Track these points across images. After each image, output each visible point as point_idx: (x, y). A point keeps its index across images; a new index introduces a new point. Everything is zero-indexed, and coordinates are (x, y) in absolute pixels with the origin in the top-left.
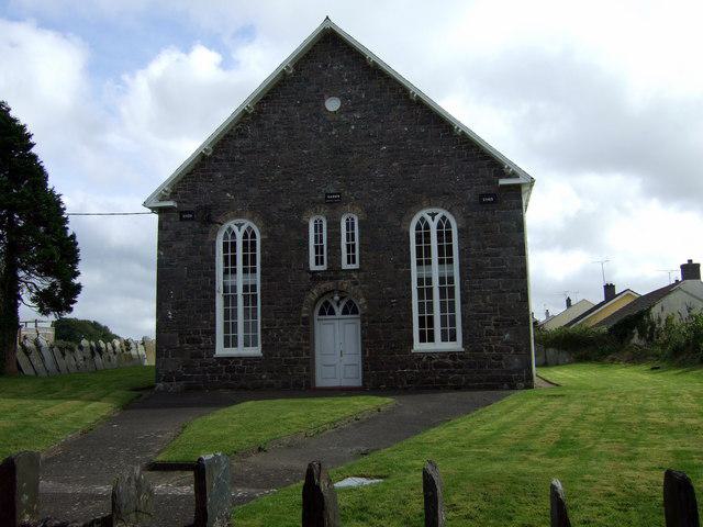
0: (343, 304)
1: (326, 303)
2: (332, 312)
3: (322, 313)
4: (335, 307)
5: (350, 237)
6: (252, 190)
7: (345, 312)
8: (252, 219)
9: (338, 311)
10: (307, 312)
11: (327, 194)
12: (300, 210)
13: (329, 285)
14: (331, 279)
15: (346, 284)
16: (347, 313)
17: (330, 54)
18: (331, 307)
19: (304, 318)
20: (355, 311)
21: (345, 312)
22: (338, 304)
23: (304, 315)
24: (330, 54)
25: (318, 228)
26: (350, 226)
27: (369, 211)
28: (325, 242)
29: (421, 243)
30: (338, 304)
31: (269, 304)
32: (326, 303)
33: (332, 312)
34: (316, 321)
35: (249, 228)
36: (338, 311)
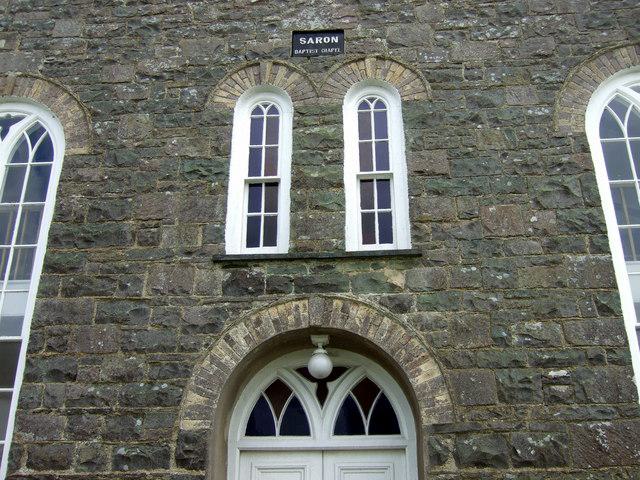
0: (339, 393)
1: (278, 390)
2: (297, 424)
3: (258, 425)
4: (310, 404)
5: (375, 154)
6: (63, 27)
7: (348, 423)
8: (46, 101)
9: (322, 419)
10: (202, 412)
11: (297, 34)
12: (208, 76)
13: (295, 311)
14: (305, 287)
15: (358, 311)
16: (357, 430)
17: (364, 243)
18: (296, 405)
19: (186, 438)
20: (386, 423)
21: (348, 423)
22: (322, 395)
23: (188, 425)
24: (364, 243)
25: (264, 128)
26: (373, 122)
27: (439, 78)
28: (284, 173)
29: (36, 170)
30: (322, 395)
31: (56, 375)
32: (278, 390)
33: (297, 424)
34: (234, 458)
35: (36, 132)
36: (322, 419)
